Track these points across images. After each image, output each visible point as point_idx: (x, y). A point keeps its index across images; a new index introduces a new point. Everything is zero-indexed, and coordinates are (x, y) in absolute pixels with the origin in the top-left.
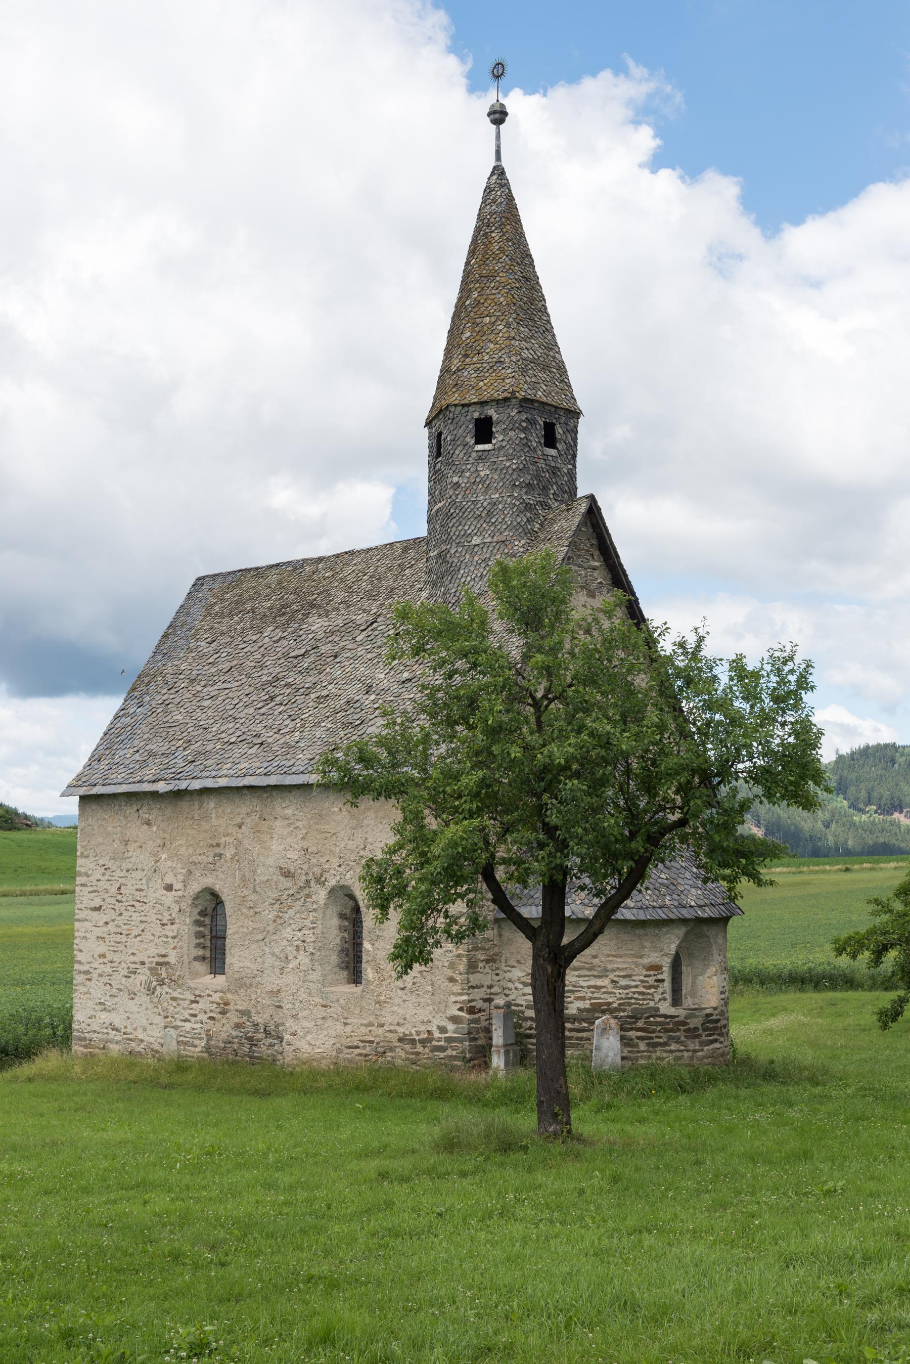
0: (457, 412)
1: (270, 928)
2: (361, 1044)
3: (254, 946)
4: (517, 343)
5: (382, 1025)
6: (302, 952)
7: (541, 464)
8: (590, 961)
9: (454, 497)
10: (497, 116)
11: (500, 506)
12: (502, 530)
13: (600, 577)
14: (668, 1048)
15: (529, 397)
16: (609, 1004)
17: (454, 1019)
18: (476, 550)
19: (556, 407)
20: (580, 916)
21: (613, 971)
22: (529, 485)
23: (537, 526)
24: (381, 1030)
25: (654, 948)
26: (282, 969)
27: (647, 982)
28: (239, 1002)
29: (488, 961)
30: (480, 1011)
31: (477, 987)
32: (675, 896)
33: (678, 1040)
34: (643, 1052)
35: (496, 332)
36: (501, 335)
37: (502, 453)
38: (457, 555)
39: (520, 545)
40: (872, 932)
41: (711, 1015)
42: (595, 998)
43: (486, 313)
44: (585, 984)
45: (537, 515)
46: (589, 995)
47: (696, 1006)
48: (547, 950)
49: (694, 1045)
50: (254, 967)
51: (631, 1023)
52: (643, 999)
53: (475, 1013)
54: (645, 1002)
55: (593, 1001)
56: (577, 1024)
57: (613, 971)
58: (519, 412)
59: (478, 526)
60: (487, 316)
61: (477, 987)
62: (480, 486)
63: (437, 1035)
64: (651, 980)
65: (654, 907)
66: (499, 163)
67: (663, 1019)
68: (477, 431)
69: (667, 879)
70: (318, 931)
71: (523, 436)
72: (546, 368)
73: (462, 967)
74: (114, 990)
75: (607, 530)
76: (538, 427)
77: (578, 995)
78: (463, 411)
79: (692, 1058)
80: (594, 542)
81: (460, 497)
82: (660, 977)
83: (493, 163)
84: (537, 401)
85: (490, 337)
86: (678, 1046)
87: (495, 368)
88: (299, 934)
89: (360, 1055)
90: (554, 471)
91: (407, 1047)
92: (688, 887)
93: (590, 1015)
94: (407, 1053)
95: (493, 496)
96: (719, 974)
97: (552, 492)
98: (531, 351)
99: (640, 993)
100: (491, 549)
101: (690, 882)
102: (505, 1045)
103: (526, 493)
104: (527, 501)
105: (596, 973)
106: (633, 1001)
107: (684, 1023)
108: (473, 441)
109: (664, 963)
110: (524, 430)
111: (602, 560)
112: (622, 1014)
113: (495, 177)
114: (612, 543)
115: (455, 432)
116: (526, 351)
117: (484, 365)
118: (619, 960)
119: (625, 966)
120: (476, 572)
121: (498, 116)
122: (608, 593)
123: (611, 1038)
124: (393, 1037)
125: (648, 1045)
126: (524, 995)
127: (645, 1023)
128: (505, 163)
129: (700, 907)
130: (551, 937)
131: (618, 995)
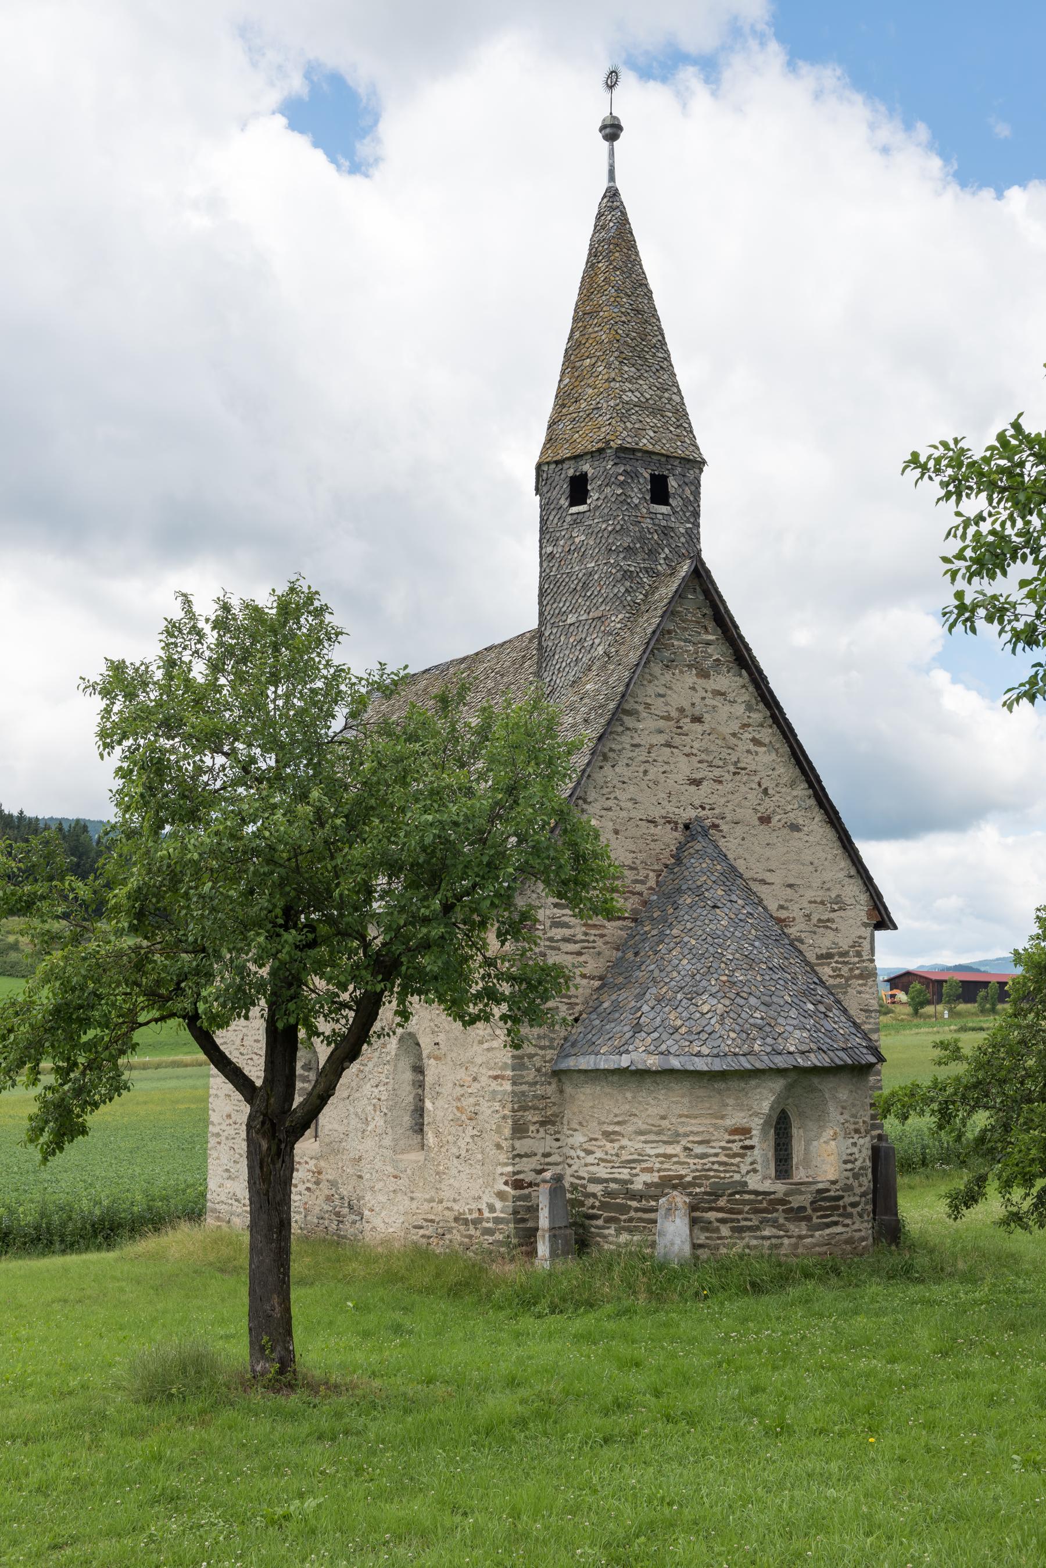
0: (551, 472)
1: (354, 1084)
2: (425, 1224)
3: (341, 1105)
4: (618, 385)
6: (378, 1113)
7: (647, 523)
9: (548, 571)
10: (608, 130)
11: (596, 577)
13: (717, 652)
14: (758, 1233)
15: (628, 446)
16: (681, 1177)
17: (501, 1195)
19: (668, 456)
20: (640, 1067)
21: (686, 1135)
22: (628, 549)
23: (641, 597)
24: (440, 1207)
25: (740, 1107)
26: (363, 1132)
27: (730, 1149)
28: (330, 1171)
29: (543, 1124)
30: (530, 1185)
31: (526, 1155)
32: (769, 1040)
34: (726, 1238)
39: (617, 620)
40: (937, 1086)
41: (828, 1190)
42: (665, 1170)
43: (587, 354)
44: (652, 1152)
45: (641, 584)
46: (657, 1165)
47: (811, 1180)
48: (261, 1118)
50: (342, 1129)
51: (710, 1202)
52: (725, 1171)
53: (522, 1188)
54: (728, 1175)
55: (662, 1174)
56: (644, 1202)
57: (686, 1135)
58: (615, 464)
61: (526, 1155)
62: (576, 555)
63: (487, 1214)
64: (735, 1147)
65: (735, 1054)
66: (611, 184)
67: (752, 1197)
69: (762, 1019)
70: (390, 1087)
71: (620, 491)
72: (657, 411)
73: (507, 1132)
74: (237, 1156)
75: (720, 596)
76: (641, 481)
77: (644, 1165)
79: (796, 1246)
81: (554, 569)
82: (747, 1143)
83: (604, 185)
84: (640, 450)
85: (589, 381)
86: (774, 1230)
89: (423, 1236)
90: (666, 532)
91: (462, 1228)
92: (790, 1029)
94: (462, 1236)
95: (589, 565)
97: (663, 556)
98: (637, 394)
99: (720, 1163)
100: (586, 627)
101: (795, 1022)
103: (624, 558)
104: (626, 568)
105: (665, 1138)
106: (712, 1173)
107: (782, 1202)
108: (567, 504)
109: (753, 1125)
110: (621, 484)
112: (698, 1190)
113: (605, 200)
115: (549, 494)
116: (629, 394)
118: (693, 1121)
119: (701, 1130)
121: (612, 131)
122: (728, 672)
123: (678, 1221)
125: (733, 1229)
126: (586, 1165)
127: (728, 1201)
128: (619, 184)
129: (803, 1053)
130: (272, 1100)
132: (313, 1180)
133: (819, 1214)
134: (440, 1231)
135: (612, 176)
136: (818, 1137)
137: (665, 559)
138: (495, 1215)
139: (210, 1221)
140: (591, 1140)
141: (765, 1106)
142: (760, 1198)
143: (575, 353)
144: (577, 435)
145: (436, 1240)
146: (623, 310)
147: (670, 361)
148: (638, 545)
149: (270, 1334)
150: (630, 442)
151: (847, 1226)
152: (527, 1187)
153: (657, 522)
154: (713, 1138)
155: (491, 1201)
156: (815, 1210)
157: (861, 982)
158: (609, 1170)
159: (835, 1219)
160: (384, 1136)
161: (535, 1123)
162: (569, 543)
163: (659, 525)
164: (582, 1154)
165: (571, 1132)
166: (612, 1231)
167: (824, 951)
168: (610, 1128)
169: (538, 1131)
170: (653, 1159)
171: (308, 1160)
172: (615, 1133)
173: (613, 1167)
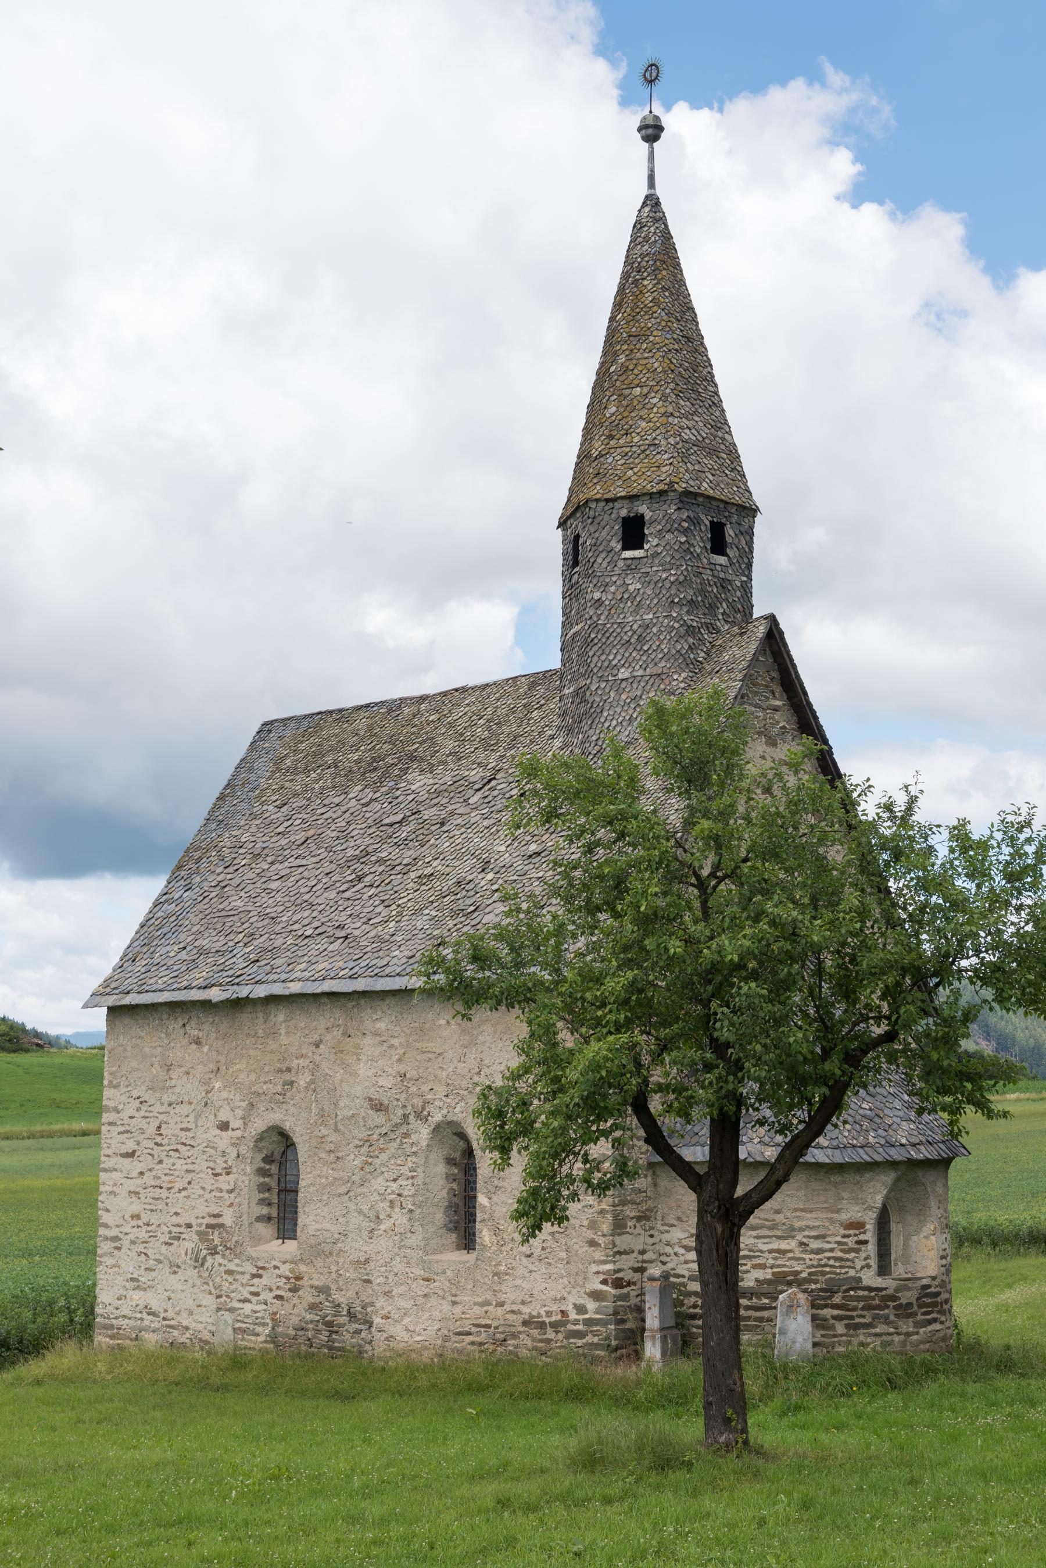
0: (599, 509)
1: (356, 1178)
2: (474, 1330)
3: (335, 1202)
5: (501, 1304)
6: (397, 1210)
7: (707, 575)
8: (772, 1217)
9: (595, 618)
10: (650, 131)
11: (655, 630)
12: (657, 660)
13: (783, 719)
14: (873, 1331)
15: (691, 489)
16: (797, 1273)
17: (596, 1295)
19: (726, 503)
20: (759, 1159)
21: (801, 1229)
23: (702, 654)
24: (500, 1311)
25: (855, 1200)
27: (845, 1244)
29: (639, 1219)
31: (625, 1253)
33: (887, 1321)
34: (841, 1335)
36: (655, 410)
38: (600, 692)
39: (680, 679)
41: (929, 1286)
42: (779, 1266)
43: (636, 382)
44: (765, 1248)
46: (771, 1261)
47: (910, 1276)
49: (906, 1326)
52: (841, 1267)
53: (622, 1287)
54: (843, 1271)
55: (775, 1270)
56: (755, 1300)
57: (801, 1229)
58: (679, 509)
59: (627, 655)
60: (638, 386)
61: (625, 1253)
63: (573, 1315)
64: (851, 1242)
65: (854, 1146)
67: (866, 1293)
69: (870, 1109)
71: (683, 539)
72: (713, 452)
73: (606, 1227)
75: (792, 660)
76: (703, 528)
77: (756, 1261)
78: (607, 508)
79: (904, 1344)
80: (775, 675)
81: (603, 617)
82: (862, 1237)
83: (642, 191)
84: (702, 495)
85: (642, 413)
87: (648, 452)
88: (394, 1186)
89: (473, 1343)
92: (898, 1120)
94: (534, 1340)
95: (645, 617)
96: (938, 1233)
97: (721, 611)
98: (694, 431)
99: (836, 1259)
100: (643, 684)
101: (901, 1114)
103: (688, 612)
105: (779, 1233)
106: (828, 1269)
107: (893, 1298)
108: (619, 547)
109: (867, 1220)
110: (685, 532)
111: (785, 697)
112: (813, 1286)
113: (647, 209)
115: (597, 534)
116: (687, 431)
117: (634, 449)
118: (809, 1215)
119: (818, 1224)
120: (623, 714)
121: (652, 132)
122: (793, 740)
123: (800, 1318)
124: (517, 1319)
125: (847, 1326)
126: (686, 1262)
127: (843, 1298)
128: (659, 192)
129: (914, 1145)
130: (721, 1186)
131: (807, 1261)
132: (288, 1286)
133: (923, 1310)
134: (499, 1336)
136: (918, 1232)
137: (722, 614)
138: (586, 1316)
139: (101, 1339)
141: (879, 1200)
142: (873, 1294)
143: (621, 379)
144: (630, 472)
145: (492, 1347)
146: (675, 336)
147: (719, 396)
148: (700, 599)
149: (734, 1408)
150: (693, 486)
152: (626, 1286)
153: (716, 573)
154: (829, 1233)
155: (582, 1301)
156: (920, 1306)
160: (409, 1235)
161: (632, 1218)
162: (622, 590)
163: (718, 577)
165: (667, 1228)
169: (635, 1227)
170: (766, 1255)
171: (279, 1264)
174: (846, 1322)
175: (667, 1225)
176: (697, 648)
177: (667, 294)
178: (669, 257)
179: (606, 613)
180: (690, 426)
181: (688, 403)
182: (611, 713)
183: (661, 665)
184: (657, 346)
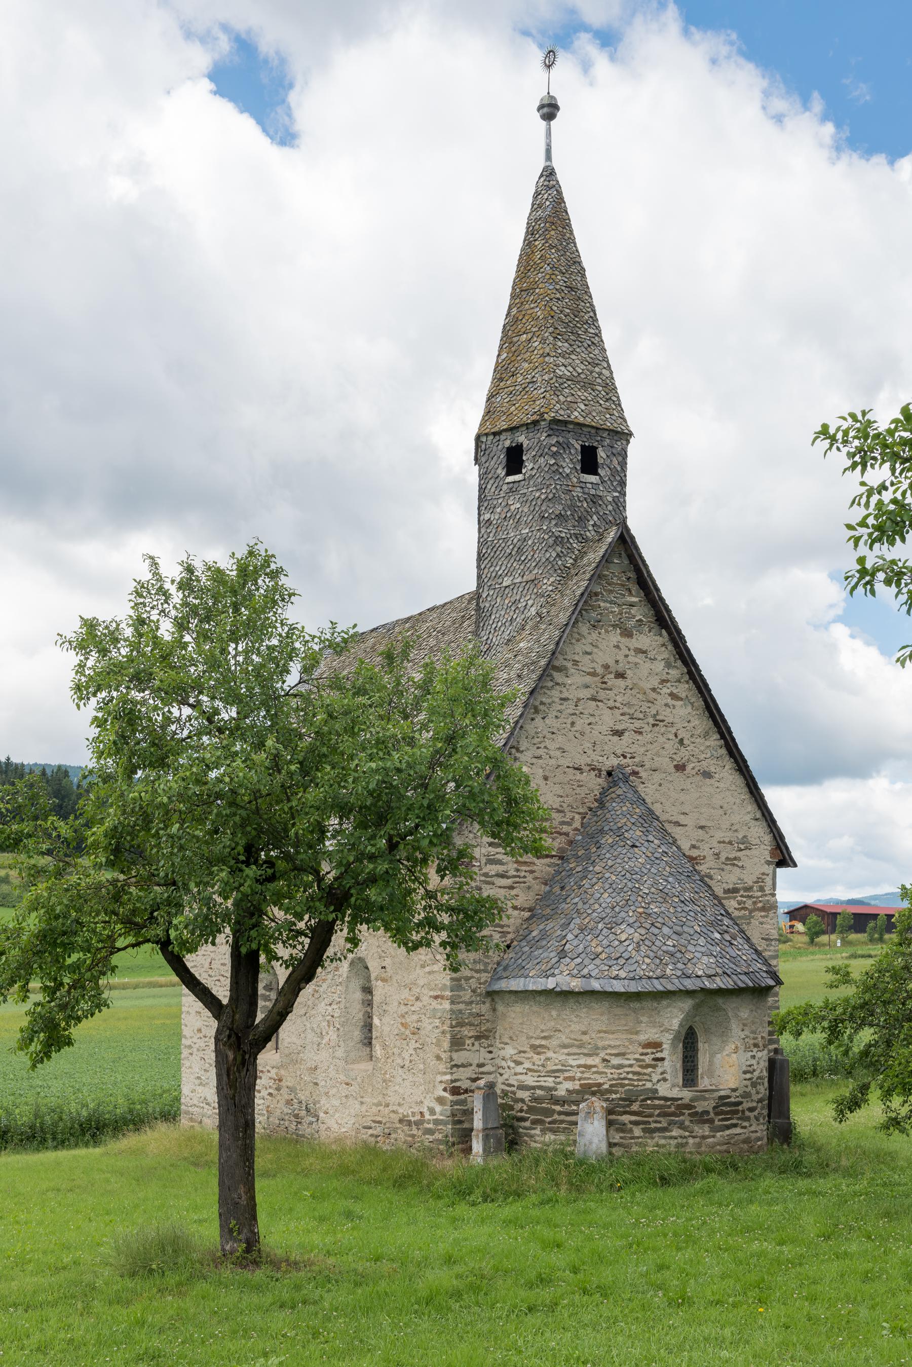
0: (489, 442)
1: (310, 1003)
2: (373, 1125)
3: (299, 1021)
5: (387, 1105)
6: (332, 1028)
7: (577, 492)
8: (579, 1037)
9: (485, 536)
10: (545, 110)
11: (530, 542)
12: (531, 568)
13: (640, 613)
14: (668, 1134)
15: (561, 418)
16: (600, 1085)
17: (440, 1100)
18: (506, 592)
19: (597, 429)
20: (564, 988)
21: (604, 1048)
22: (560, 516)
23: (571, 561)
24: (387, 1110)
25: (653, 1024)
27: (643, 1060)
29: (478, 1038)
31: (463, 1066)
32: (680, 965)
33: (682, 1126)
34: (638, 1138)
35: (531, 350)
36: (535, 352)
37: (531, 483)
38: (489, 599)
39: (549, 583)
41: (729, 1097)
42: (585, 1079)
43: (523, 330)
44: (574, 1063)
46: (579, 1075)
47: (714, 1088)
49: (706, 1130)
50: (299, 1042)
51: (624, 1107)
52: (638, 1080)
54: (640, 1083)
55: (582, 1082)
56: (566, 1107)
57: (604, 1048)
58: (549, 435)
59: (509, 565)
60: (524, 333)
61: (463, 1066)
62: (511, 521)
63: (427, 1116)
64: (648, 1059)
65: (649, 978)
67: (662, 1102)
68: (508, 461)
69: (674, 946)
70: (342, 1005)
71: (552, 462)
72: (588, 385)
73: (446, 1045)
74: (207, 1065)
75: (643, 561)
76: (573, 451)
78: (494, 441)
79: (699, 1145)
80: (632, 575)
81: (491, 535)
82: (659, 1055)
83: (541, 164)
84: (572, 422)
85: (525, 356)
87: (527, 389)
88: (330, 1008)
89: (372, 1135)
92: (698, 955)
93: (579, 1097)
94: (406, 1135)
95: (523, 532)
96: (741, 1051)
97: (592, 523)
99: (634, 1073)
100: (521, 589)
101: (703, 949)
102: (484, 1129)
103: (556, 525)
104: (557, 534)
105: (586, 1051)
106: (626, 1082)
107: (688, 1107)
108: (504, 473)
109: (664, 1040)
111: (643, 594)
112: (614, 1096)
113: (542, 179)
114: (650, 575)
115: (487, 464)
116: (563, 368)
117: (517, 388)
118: (611, 1036)
119: (618, 1043)
120: (506, 616)
121: (549, 110)
122: (650, 631)
123: (596, 1123)
124: (395, 1118)
125: (644, 1130)
126: (516, 1074)
127: (641, 1106)
128: (556, 164)
129: (710, 976)
130: (237, 1017)
131: (609, 1075)
133: (720, 1117)
134: (387, 1131)
135: (548, 157)
136: (721, 1050)
137: (593, 526)
138: (435, 1117)
139: (184, 1121)
140: (520, 1052)
142: (669, 1103)
143: (512, 328)
146: (558, 287)
148: (569, 513)
149: (238, 1219)
150: (563, 415)
151: (745, 1127)
153: (586, 490)
154: (629, 1051)
156: (717, 1114)
157: (763, 914)
158: (536, 1079)
159: (734, 1121)
161: (471, 1037)
163: (588, 494)
164: (512, 1065)
165: (503, 1045)
166: (538, 1132)
167: (731, 886)
168: (538, 1042)
169: (473, 1044)
170: (575, 1069)
171: (270, 1069)
172: (541, 1046)
173: (539, 1076)
174: (643, 1126)
175: (503, 1043)
176: (565, 556)
177: (553, 251)
178: (559, 219)
179: (494, 531)
180: (566, 363)
181: (566, 345)
182: (498, 616)
183: (535, 572)
184: (541, 297)
